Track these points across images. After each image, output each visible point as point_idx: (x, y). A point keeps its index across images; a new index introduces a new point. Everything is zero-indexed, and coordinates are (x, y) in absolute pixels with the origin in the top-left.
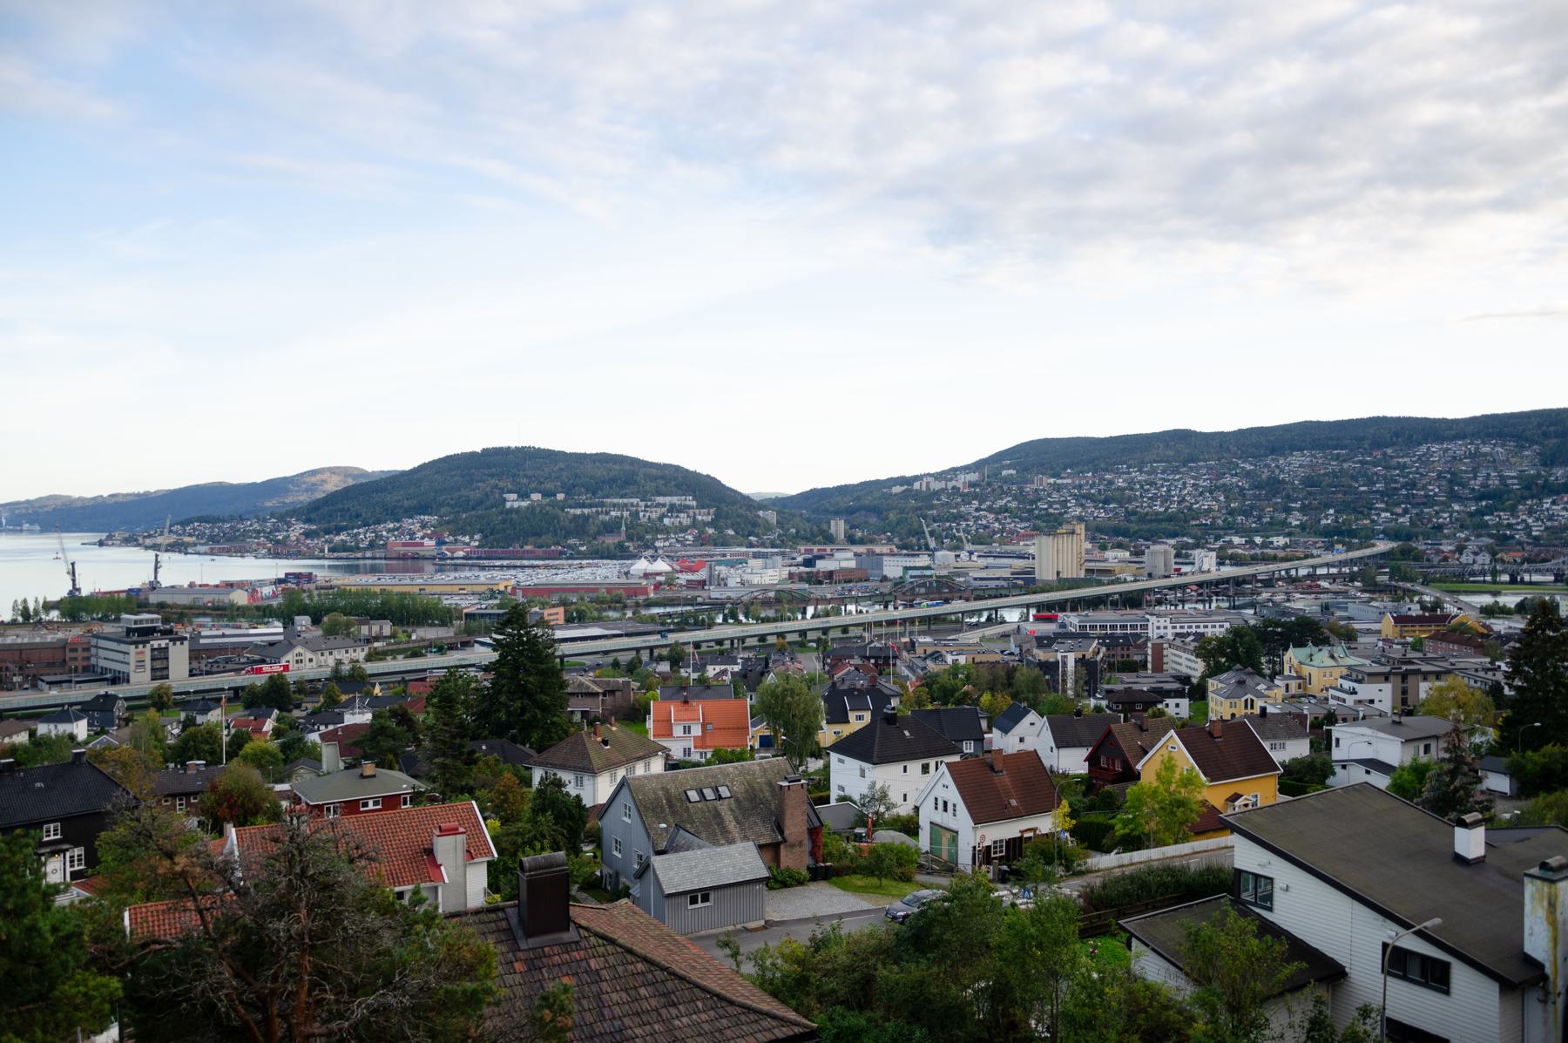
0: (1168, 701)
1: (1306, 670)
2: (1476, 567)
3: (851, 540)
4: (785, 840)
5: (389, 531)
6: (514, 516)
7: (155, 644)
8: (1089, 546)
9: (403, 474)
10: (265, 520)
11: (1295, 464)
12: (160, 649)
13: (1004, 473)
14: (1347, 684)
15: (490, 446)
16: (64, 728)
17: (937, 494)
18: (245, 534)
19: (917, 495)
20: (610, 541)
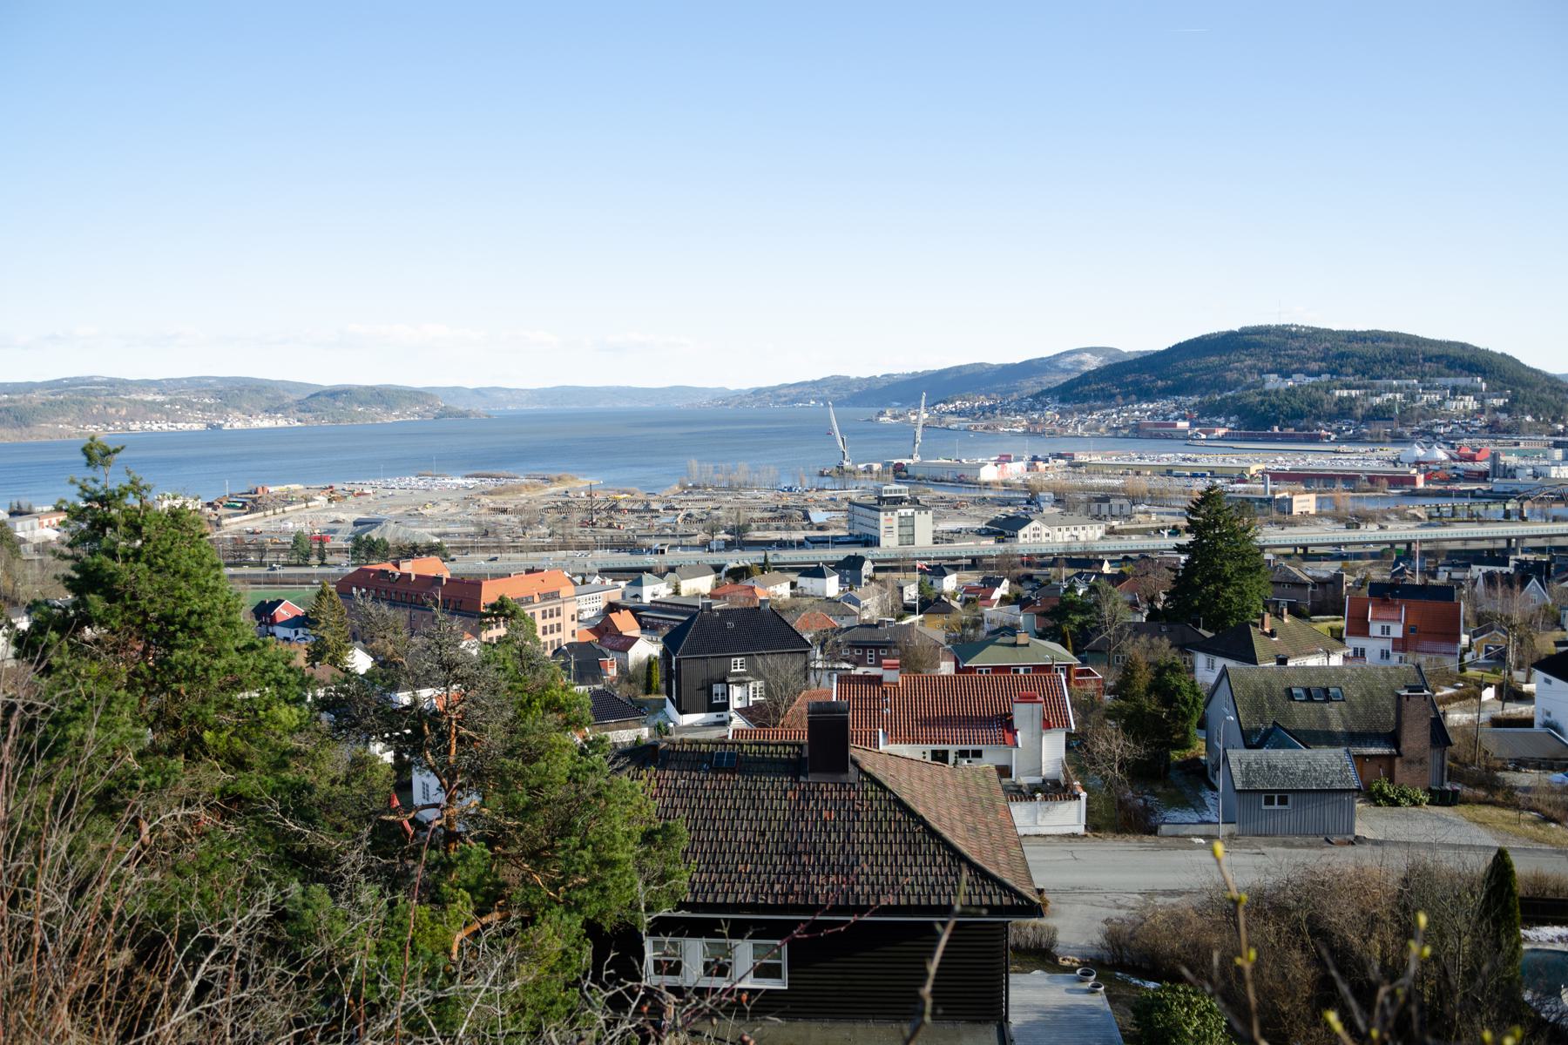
4: (1399, 754)
6: (1273, 398)
7: (902, 512)
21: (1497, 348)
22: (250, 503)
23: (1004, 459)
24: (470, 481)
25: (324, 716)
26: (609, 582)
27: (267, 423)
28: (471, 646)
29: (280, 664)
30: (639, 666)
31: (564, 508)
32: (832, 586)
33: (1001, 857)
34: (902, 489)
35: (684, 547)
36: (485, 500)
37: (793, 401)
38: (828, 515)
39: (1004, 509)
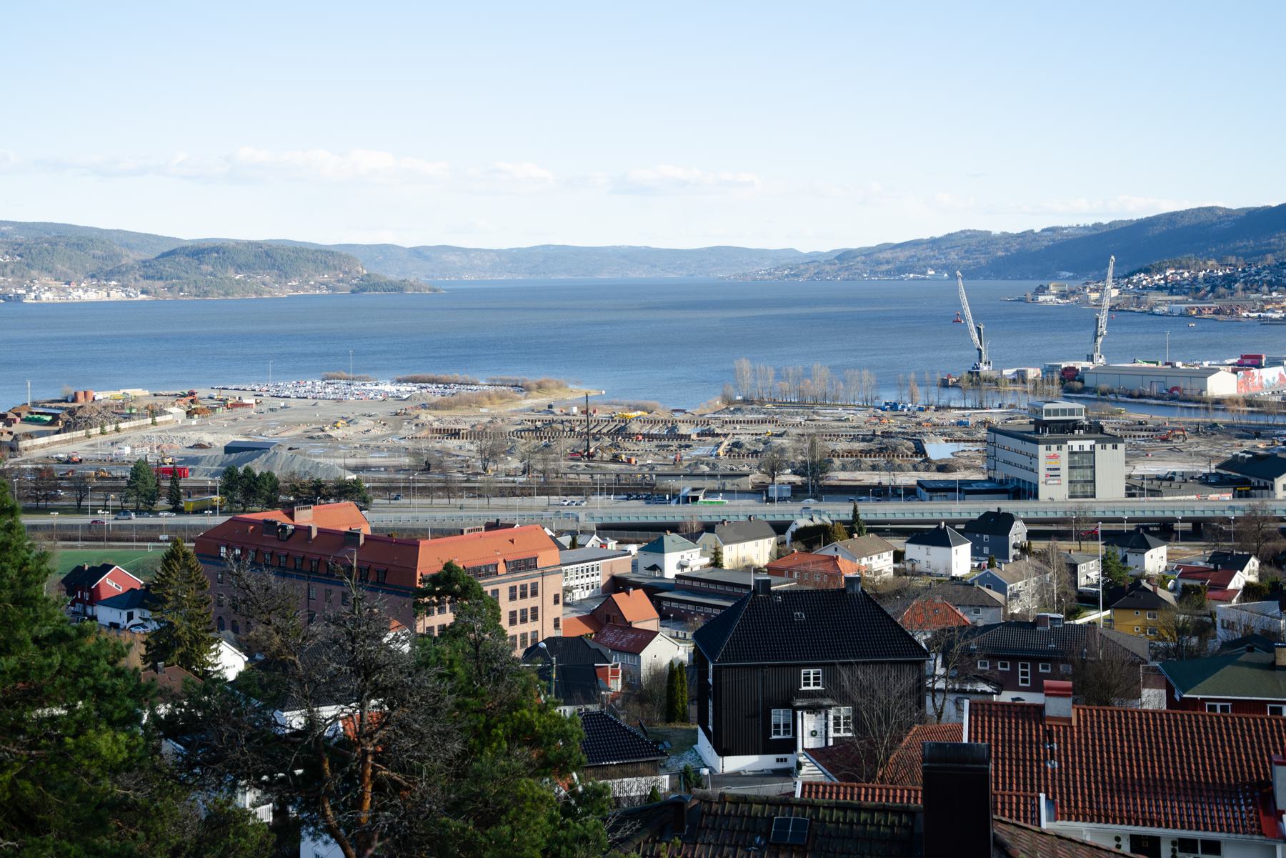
7: (1076, 445)
12: (1081, 452)
22: (65, 416)
23: (1251, 362)
24: (404, 388)
25: (168, 746)
26: (612, 545)
27: (93, 296)
28: (398, 642)
29: (103, 664)
30: (656, 675)
31: (544, 430)
32: (961, 560)
34: (1076, 409)
35: (728, 493)
36: (426, 416)
37: (901, 270)
38: (954, 447)
39: (1248, 444)
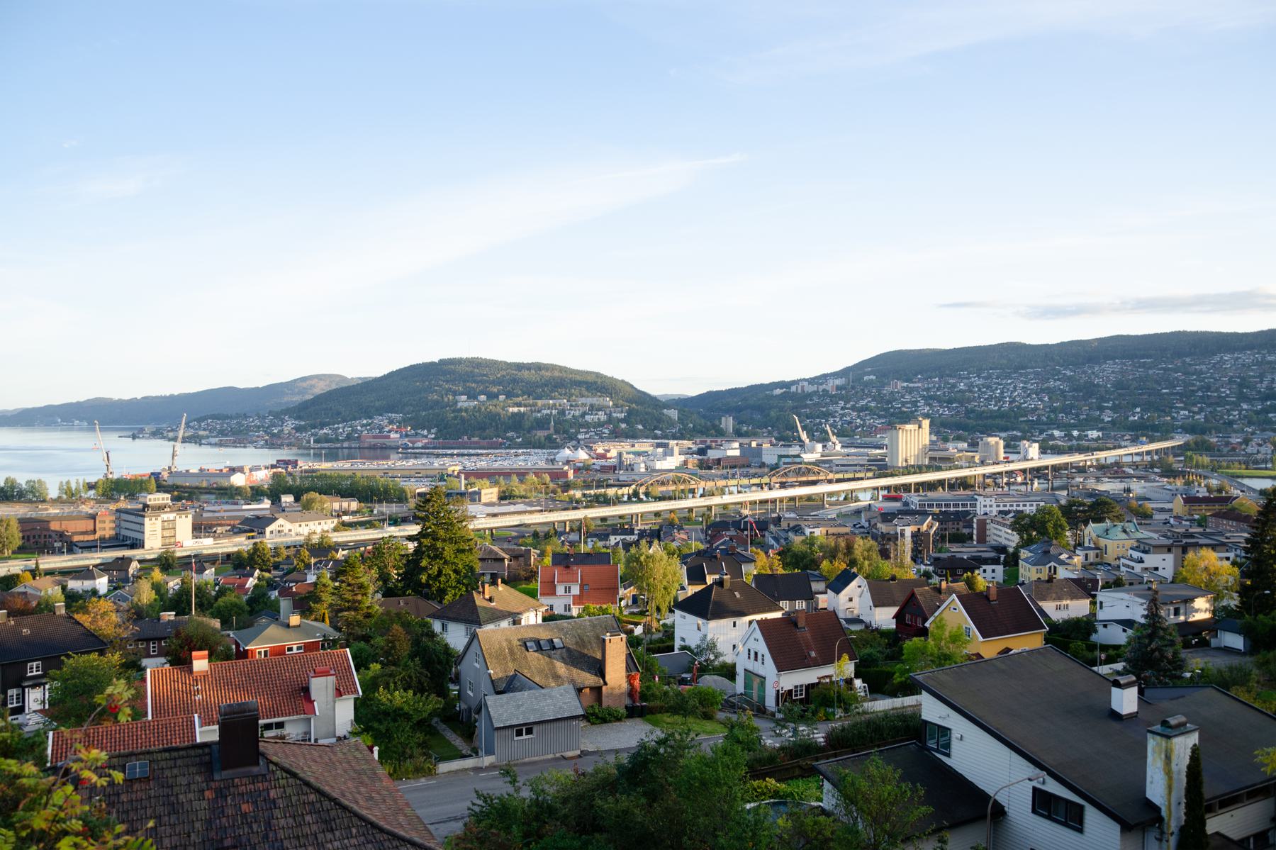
0: (984, 567)
1: (1103, 542)
2: (1260, 456)
3: (739, 434)
5: (363, 426)
7: (165, 516)
8: (934, 438)
9: (376, 380)
10: (264, 418)
11: (1106, 373)
13: (866, 378)
14: (1136, 554)
15: (446, 357)
16: (87, 584)
17: (809, 396)
18: (248, 429)
19: (793, 396)
20: (541, 434)
21: (619, 376)
33: (401, 818)
